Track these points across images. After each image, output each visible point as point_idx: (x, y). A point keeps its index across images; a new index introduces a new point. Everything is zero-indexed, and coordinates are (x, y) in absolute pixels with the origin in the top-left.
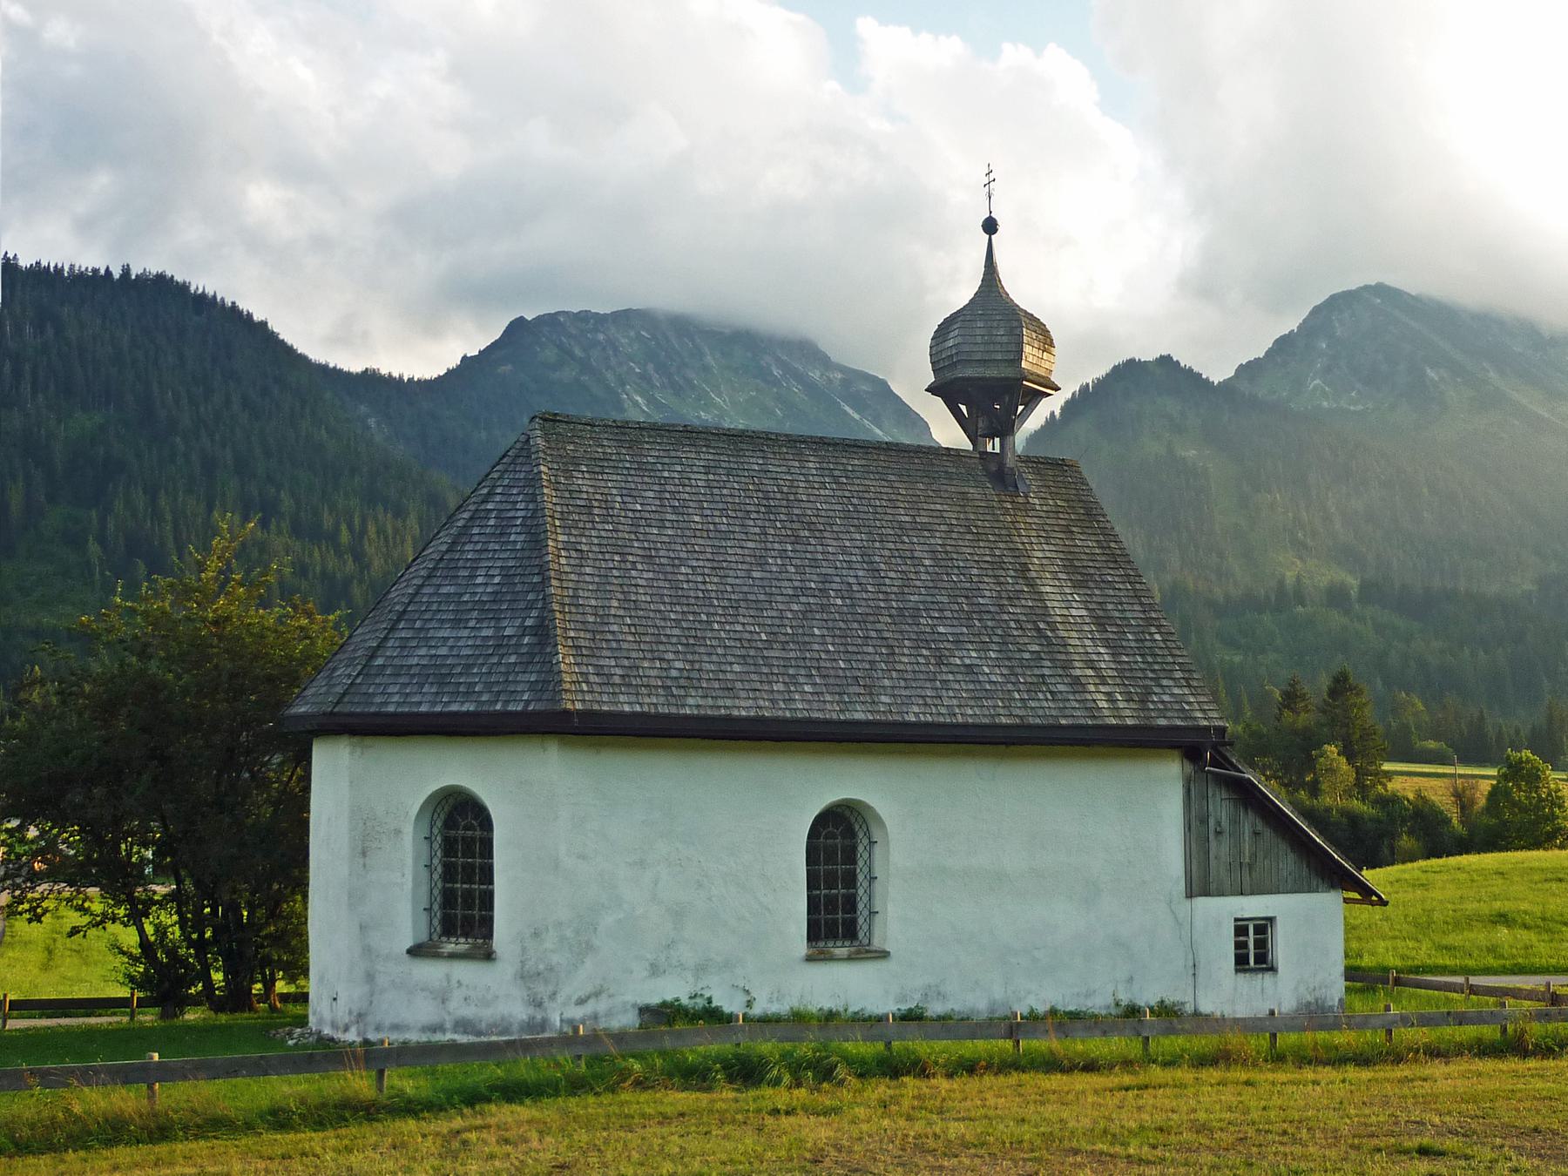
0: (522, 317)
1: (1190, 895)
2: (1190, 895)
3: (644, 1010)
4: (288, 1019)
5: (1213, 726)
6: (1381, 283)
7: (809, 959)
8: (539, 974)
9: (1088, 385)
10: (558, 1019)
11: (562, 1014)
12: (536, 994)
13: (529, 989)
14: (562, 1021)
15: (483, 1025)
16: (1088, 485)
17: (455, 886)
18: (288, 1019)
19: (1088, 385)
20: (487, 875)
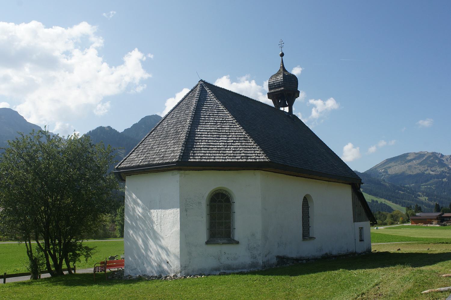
0: (268, 98)
1: (354, 222)
2: (354, 222)
3: (278, 257)
4: (58, 283)
5: (221, 193)
6: (101, 129)
7: (303, 240)
8: (254, 248)
9: (91, 131)
10: (261, 262)
11: (262, 260)
12: (254, 254)
13: (251, 253)
14: (262, 262)
15: (235, 266)
16: (437, 153)
17: (225, 221)
18: (58, 283)
19: (91, 131)
20: (448, 213)
